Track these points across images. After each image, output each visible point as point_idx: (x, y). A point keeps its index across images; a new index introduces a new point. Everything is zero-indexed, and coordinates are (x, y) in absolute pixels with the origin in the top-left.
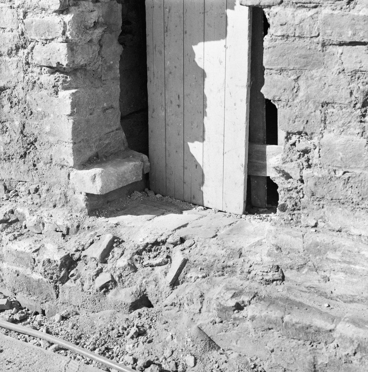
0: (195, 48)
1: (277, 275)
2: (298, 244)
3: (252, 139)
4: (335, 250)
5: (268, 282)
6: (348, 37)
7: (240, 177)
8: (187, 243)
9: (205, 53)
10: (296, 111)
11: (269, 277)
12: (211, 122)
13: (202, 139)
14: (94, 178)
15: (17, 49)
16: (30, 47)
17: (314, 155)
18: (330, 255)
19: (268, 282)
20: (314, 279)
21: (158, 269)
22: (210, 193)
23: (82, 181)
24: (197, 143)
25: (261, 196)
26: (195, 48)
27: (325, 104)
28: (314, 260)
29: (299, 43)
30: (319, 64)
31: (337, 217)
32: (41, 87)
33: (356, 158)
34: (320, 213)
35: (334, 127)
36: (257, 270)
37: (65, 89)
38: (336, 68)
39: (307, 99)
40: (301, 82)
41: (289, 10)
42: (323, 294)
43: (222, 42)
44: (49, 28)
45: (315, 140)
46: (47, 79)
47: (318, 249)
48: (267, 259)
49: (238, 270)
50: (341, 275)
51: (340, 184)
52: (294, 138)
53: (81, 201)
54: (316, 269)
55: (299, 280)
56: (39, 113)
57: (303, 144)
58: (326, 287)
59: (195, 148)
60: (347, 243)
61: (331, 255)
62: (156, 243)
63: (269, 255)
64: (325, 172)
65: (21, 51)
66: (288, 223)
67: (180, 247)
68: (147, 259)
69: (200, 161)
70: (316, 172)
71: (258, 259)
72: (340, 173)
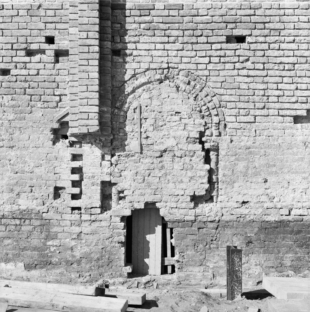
0: (146, 236)
1: (180, 283)
2: (183, 275)
3: (162, 257)
4: (192, 275)
5: (178, 285)
6: (191, 233)
7: (160, 266)
8: (156, 281)
9: (149, 237)
10: (181, 248)
11: (178, 283)
12: (151, 253)
13: (148, 257)
14: (129, 269)
15: (109, 238)
16: (113, 237)
17: (185, 257)
18: (191, 276)
19: (178, 285)
20: (188, 282)
21: (151, 287)
22: (151, 271)
23: (126, 270)
24: (147, 259)
25: (164, 270)
26: (146, 236)
27: (187, 246)
28: (187, 278)
29: (182, 235)
30: (186, 238)
31: (191, 268)
32: (116, 247)
33: (194, 256)
34: (186, 269)
35: (189, 250)
36: (175, 283)
37: (122, 247)
38: (189, 239)
39: (184, 245)
40: (182, 242)
41: (179, 229)
42: (190, 285)
43: (154, 235)
44: (120, 233)
45: (185, 253)
46: (117, 245)
47: (188, 275)
48: (177, 280)
49: (171, 283)
50: (193, 280)
51: (191, 262)
52: (180, 254)
53: (126, 275)
54: (188, 280)
55: (184, 283)
56: (114, 254)
57: (183, 254)
58: (190, 283)
59: (146, 260)
60: (194, 273)
61: (191, 276)
62: (148, 282)
63: (177, 279)
64: (188, 260)
65: (110, 239)
66: (180, 271)
67: (154, 282)
68: (147, 285)
69: (148, 263)
70: (186, 260)
71: (175, 280)
72: (191, 259)
